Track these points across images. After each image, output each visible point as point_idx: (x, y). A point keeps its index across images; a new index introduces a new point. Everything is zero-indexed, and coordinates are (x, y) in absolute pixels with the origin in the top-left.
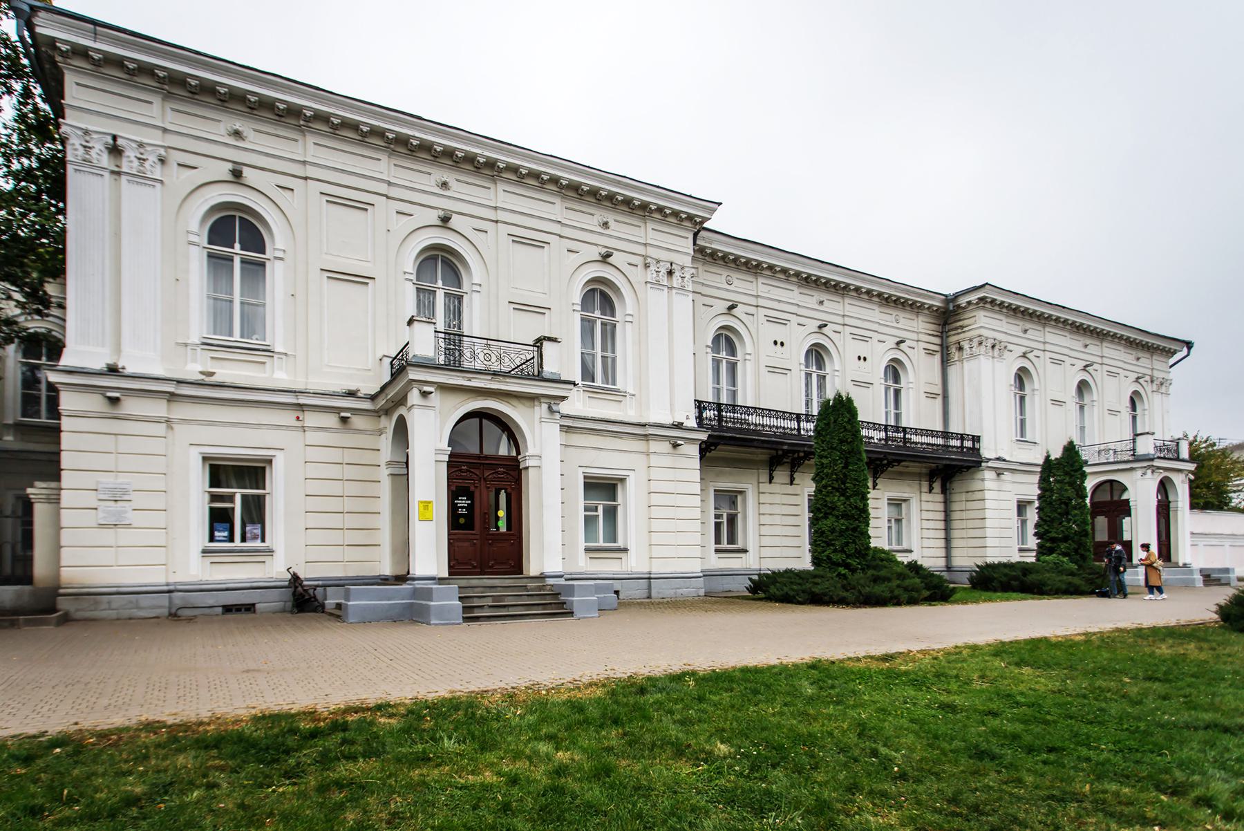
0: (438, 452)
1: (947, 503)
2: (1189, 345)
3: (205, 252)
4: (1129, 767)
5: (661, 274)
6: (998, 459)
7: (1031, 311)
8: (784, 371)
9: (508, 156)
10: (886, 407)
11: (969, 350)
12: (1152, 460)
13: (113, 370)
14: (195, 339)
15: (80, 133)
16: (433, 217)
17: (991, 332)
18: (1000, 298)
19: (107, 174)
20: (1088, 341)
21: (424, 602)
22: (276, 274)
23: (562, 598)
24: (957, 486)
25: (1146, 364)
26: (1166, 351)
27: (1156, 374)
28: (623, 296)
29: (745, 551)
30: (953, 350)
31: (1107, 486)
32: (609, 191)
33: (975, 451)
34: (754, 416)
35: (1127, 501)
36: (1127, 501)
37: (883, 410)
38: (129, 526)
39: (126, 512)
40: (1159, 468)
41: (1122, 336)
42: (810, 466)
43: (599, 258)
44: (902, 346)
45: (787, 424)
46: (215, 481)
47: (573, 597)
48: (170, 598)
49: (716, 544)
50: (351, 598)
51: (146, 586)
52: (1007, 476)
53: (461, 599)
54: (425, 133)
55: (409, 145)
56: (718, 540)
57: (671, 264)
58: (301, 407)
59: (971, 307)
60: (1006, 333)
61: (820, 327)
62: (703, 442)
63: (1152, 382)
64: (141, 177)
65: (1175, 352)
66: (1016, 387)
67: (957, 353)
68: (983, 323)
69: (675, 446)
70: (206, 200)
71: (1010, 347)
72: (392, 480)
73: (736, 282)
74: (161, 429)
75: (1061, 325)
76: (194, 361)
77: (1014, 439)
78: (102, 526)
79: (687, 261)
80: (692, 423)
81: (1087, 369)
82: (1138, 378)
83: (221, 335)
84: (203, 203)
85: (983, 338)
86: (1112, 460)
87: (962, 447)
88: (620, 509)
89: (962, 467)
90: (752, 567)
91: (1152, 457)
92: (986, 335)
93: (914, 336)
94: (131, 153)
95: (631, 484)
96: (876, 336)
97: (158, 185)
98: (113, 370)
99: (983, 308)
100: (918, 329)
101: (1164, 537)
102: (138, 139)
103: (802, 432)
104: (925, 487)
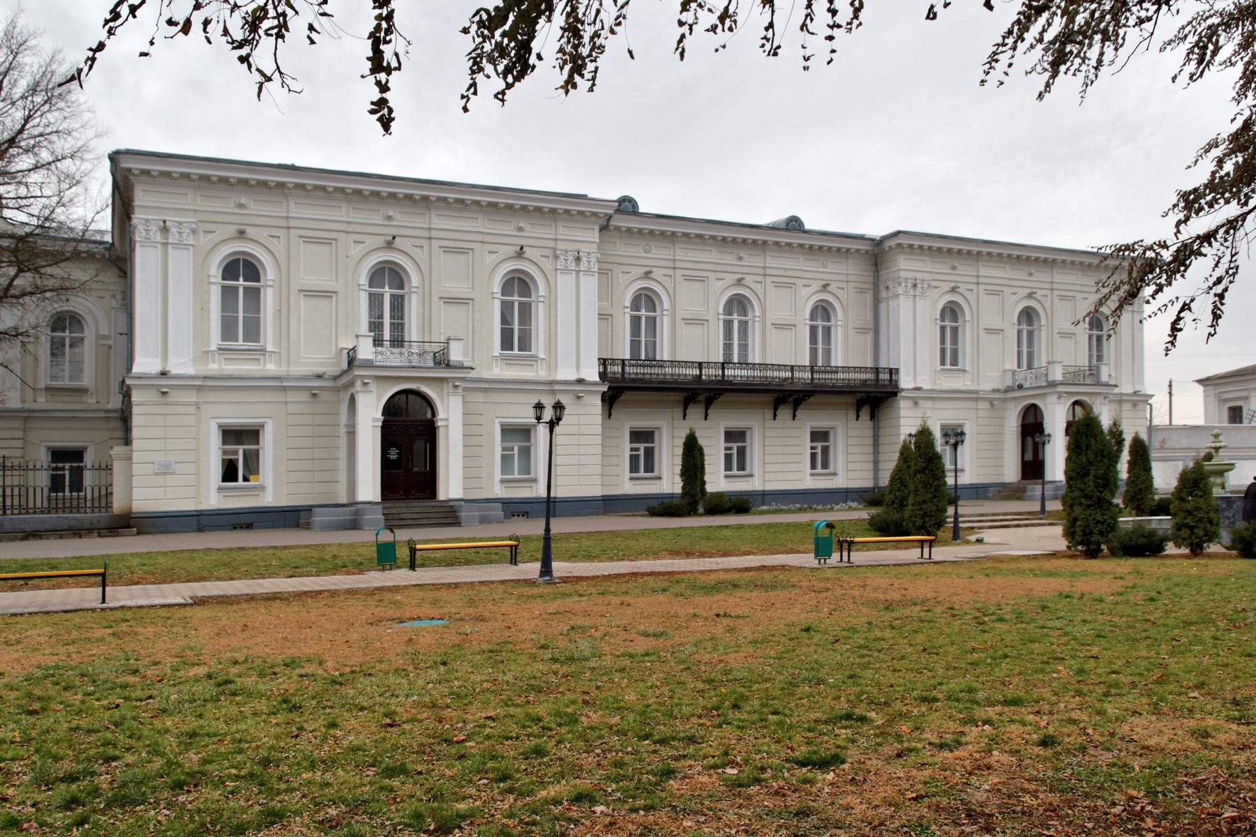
1: (876, 429)
3: (220, 287)
4: (413, 762)
8: (701, 322)
10: (1019, 346)
13: (164, 374)
14: (213, 347)
19: (159, 246)
22: (269, 300)
30: (882, 288)
37: (1087, 353)
38: (173, 473)
42: (700, 402)
43: (386, 245)
46: (225, 440)
48: (198, 521)
49: (631, 472)
56: (813, 466)
58: (284, 389)
62: (604, 392)
64: (180, 246)
68: (905, 267)
73: (959, 267)
76: (213, 361)
78: (156, 474)
88: (532, 449)
97: (191, 248)
98: (164, 374)
102: (145, 217)
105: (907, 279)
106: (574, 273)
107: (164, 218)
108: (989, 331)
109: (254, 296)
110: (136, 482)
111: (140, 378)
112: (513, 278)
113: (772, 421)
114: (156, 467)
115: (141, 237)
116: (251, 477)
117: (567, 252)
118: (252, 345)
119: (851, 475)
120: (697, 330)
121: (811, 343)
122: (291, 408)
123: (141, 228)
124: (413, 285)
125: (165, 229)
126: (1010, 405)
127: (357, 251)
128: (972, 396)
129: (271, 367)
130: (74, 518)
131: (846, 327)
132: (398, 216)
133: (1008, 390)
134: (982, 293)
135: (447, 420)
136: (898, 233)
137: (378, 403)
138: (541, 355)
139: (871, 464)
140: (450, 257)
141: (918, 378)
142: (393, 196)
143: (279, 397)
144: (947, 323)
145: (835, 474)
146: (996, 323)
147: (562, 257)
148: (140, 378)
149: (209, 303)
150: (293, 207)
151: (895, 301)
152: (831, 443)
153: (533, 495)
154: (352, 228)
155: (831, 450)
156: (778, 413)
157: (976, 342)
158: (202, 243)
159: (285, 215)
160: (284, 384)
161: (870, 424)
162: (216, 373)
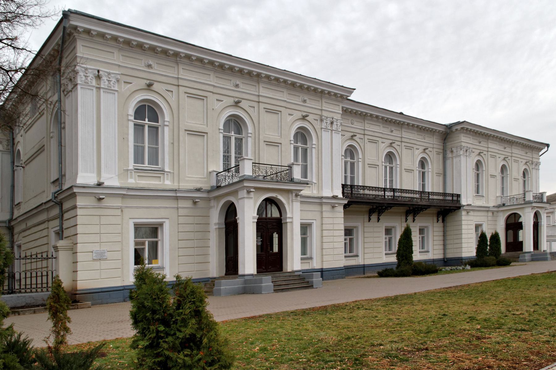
0: (254, 218)
2: (548, 145)
5: (328, 124)
6: (468, 205)
7: (479, 132)
9: (266, 71)
11: (456, 152)
12: (532, 203)
13: (100, 185)
14: (131, 167)
15: (83, 69)
16: (143, 83)
17: (466, 144)
18: (470, 128)
19: (94, 89)
20: (481, 140)
21: (259, 285)
22: (166, 135)
23: (307, 280)
24: (449, 219)
25: (529, 155)
26: (536, 148)
27: (325, 114)
28: (312, 137)
29: (357, 256)
31: (513, 216)
32: (249, 70)
33: (458, 201)
34: (366, 190)
35: (521, 223)
36: (521, 223)
38: (106, 259)
39: (105, 253)
40: (534, 207)
41: (520, 142)
43: (234, 104)
44: (427, 151)
45: (415, 196)
47: (262, 283)
50: (263, 283)
51: (89, 290)
52: (471, 213)
53: (272, 282)
54: (231, 62)
55: (156, 50)
57: (333, 119)
59: (458, 132)
60: (472, 144)
61: (352, 136)
63: (532, 164)
64: (109, 90)
65: (542, 149)
66: (475, 170)
67: (450, 154)
68: (465, 140)
69: (333, 207)
70: (136, 99)
71: (474, 150)
72: (219, 231)
74: (118, 212)
75: (495, 139)
76: (131, 178)
77: (474, 195)
78: (94, 260)
79: (338, 117)
80: (340, 196)
81: (506, 159)
82: (526, 162)
83: (153, 165)
84: (134, 100)
85: (463, 147)
86: (515, 204)
87: (452, 200)
89: (453, 209)
90: (361, 264)
91: (532, 201)
92: (463, 145)
93: (431, 146)
94: (105, 78)
95: (166, 227)
96: (415, 147)
97: (116, 93)
98: (100, 185)
99: (463, 133)
100: (433, 143)
101: (536, 239)
102: (108, 71)
103: (386, 197)
104: (435, 220)
105: (464, 147)
106: (330, 131)
107: (98, 68)
108: (192, 133)
109: (154, 130)
110: (79, 266)
111: (84, 187)
112: (299, 132)
113: (412, 223)
114: (94, 255)
115: (81, 81)
116: (153, 261)
117: (327, 118)
118: (154, 167)
119: (435, 252)
120: (373, 170)
121: (479, 185)
122: (181, 212)
123: (81, 74)
124: (166, 119)
125: (98, 77)
126: (501, 214)
127: (218, 106)
128: (486, 209)
129: (168, 183)
130: (30, 297)
131: (433, 172)
132: (241, 85)
133: (499, 206)
134: (262, 111)
135: (292, 218)
136: (459, 123)
137: (254, 208)
138: (314, 181)
139: (442, 246)
140: (270, 115)
141: (468, 200)
142: (115, 39)
143: (172, 204)
144: (299, 144)
145: (428, 252)
146: (274, 137)
147: (325, 121)
148: (84, 187)
149: (128, 134)
150: (261, 89)
151: (458, 159)
152: (354, 236)
153: (310, 268)
154: (215, 90)
155: (426, 238)
156: (371, 217)
157: (175, 143)
158: (123, 90)
159: (177, 76)
160: (178, 195)
161: (440, 224)
162: (134, 186)
